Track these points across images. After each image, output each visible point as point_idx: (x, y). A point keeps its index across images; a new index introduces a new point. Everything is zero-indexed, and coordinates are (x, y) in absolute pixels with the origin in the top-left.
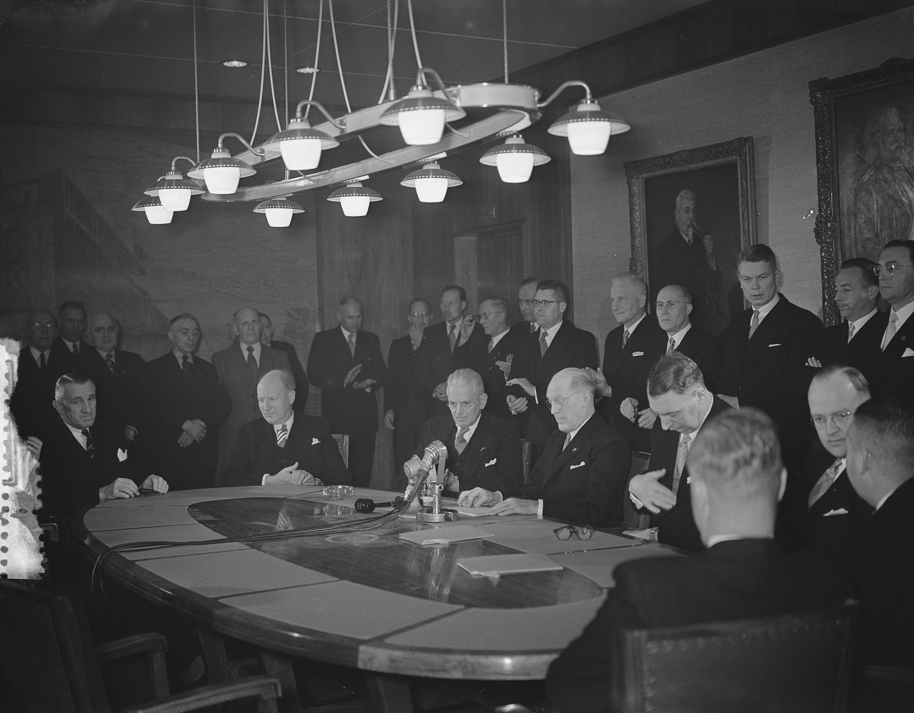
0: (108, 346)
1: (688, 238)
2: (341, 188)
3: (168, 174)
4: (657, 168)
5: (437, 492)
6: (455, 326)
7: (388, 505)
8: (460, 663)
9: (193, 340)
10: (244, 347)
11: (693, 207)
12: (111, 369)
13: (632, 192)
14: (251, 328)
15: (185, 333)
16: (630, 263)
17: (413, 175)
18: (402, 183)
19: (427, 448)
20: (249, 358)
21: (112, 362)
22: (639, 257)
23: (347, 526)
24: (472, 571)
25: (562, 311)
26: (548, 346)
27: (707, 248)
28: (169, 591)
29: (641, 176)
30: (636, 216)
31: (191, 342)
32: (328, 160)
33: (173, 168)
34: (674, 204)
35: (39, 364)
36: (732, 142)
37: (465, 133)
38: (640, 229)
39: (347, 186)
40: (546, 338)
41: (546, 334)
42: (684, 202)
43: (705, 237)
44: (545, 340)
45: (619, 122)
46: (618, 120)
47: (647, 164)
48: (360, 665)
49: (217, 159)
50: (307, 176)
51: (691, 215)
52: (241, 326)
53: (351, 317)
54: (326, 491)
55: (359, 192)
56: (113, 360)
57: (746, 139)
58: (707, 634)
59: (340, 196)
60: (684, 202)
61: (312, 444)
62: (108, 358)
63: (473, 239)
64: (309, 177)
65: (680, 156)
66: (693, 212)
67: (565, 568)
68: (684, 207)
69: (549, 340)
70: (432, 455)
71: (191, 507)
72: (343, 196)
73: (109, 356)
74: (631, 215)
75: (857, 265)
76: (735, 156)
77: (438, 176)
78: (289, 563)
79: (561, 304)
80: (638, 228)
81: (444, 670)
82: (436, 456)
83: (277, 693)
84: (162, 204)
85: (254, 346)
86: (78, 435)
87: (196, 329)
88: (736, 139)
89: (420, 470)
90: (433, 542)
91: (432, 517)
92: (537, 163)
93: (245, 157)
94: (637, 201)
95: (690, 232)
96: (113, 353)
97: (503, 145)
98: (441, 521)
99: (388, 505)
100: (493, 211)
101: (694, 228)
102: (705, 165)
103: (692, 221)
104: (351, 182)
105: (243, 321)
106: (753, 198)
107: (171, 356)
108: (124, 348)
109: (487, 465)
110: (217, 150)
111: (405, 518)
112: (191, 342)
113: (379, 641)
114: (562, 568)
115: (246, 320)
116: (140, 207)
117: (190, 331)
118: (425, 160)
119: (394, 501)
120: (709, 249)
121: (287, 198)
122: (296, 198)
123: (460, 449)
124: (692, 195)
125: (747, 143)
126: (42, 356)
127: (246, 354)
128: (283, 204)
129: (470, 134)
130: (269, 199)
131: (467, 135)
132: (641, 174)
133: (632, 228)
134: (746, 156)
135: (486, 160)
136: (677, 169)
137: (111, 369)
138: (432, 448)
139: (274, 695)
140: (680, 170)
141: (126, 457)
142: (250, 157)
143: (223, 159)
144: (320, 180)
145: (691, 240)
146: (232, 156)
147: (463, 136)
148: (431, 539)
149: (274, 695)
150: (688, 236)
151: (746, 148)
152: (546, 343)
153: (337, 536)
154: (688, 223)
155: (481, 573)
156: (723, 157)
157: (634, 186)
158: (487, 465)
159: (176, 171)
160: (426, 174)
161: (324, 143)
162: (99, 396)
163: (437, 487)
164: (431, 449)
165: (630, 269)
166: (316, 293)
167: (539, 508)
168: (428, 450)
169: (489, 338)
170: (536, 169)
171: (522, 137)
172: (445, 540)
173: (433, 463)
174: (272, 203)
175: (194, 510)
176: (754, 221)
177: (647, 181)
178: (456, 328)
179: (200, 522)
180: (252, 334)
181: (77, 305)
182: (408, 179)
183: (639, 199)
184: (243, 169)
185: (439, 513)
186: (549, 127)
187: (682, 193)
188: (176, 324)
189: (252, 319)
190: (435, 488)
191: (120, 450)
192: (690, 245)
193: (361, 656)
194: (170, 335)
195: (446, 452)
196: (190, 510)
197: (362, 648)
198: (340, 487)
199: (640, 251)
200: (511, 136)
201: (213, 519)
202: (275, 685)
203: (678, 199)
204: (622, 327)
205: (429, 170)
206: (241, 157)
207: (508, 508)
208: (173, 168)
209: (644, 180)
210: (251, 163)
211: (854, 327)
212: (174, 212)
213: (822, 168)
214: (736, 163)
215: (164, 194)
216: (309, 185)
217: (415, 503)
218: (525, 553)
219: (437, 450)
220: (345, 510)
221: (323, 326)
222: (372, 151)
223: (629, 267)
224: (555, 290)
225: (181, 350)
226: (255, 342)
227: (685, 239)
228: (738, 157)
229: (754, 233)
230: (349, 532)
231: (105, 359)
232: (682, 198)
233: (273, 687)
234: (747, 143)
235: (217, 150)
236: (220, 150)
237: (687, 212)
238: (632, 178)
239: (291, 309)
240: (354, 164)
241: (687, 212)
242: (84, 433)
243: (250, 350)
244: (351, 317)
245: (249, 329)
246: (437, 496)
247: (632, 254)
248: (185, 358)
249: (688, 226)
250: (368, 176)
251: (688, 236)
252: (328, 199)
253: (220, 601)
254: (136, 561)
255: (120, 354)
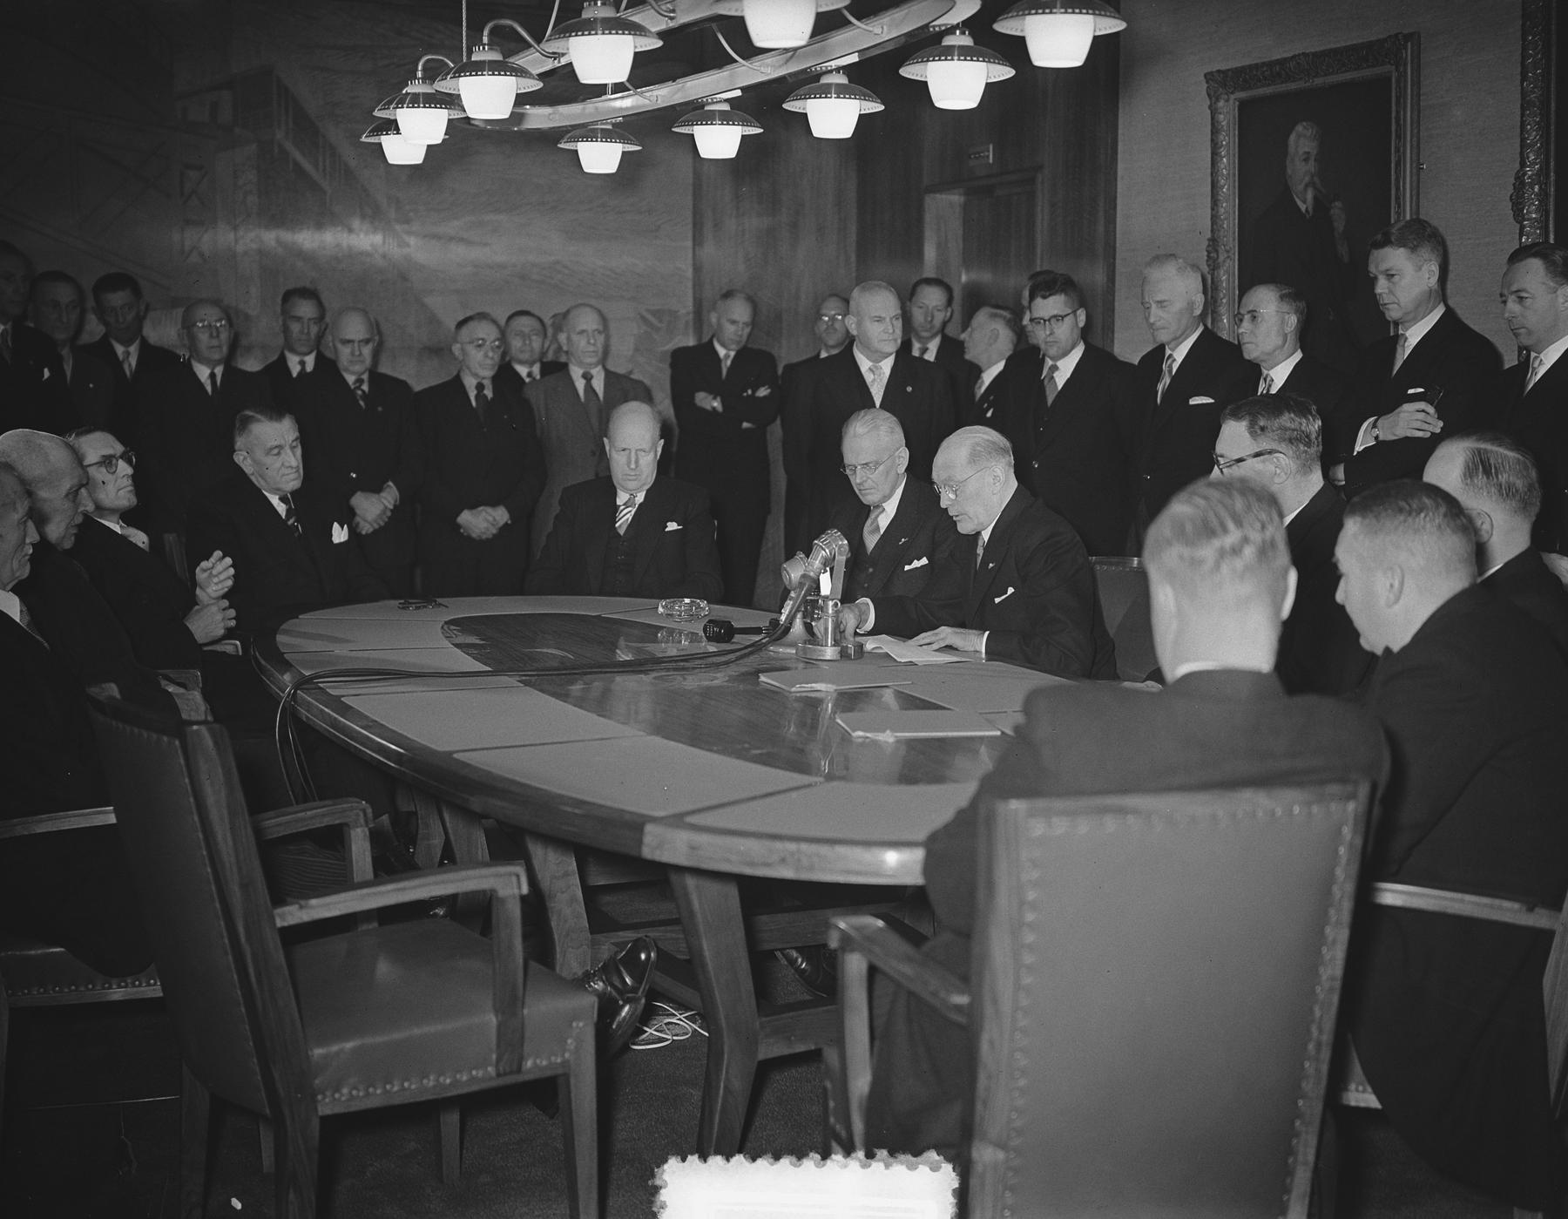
0: (358, 368)
1: (1305, 206)
2: (697, 111)
3: (411, 83)
4: (1259, 84)
5: (830, 611)
6: (927, 349)
7: (757, 631)
8: (792, 854)
9: (492, 358)
10: (576, 372)
11: (1315, 152)
12: (362, 403)
13: (1216, 124)
14: (592, 341)
15: (480, 346)
16: (1209, 246)
17: (802, 93)
18: (784, 106)
19: (816, 542)
20: (586, 391)
21: (363, 391)
22: (1224, 237)
23: (682, 661)
24: (854, 731)
25: (1081, 324)
26: (1060, 388)
27: (1336, 224)
28: (393, 744)
29: (1232, 97)
30: (1222, 166)
31: (489, 362)
32: (646, 70)
33: (419, 74)
34: (1286, 146)
35: (209, 389)
36: (1385, 40)
37: (873, 26)
38: (1228, 189)
39: (706, 108)
40: (1055, 375)
41: (1054, 368)
42: (1302, 142)
43: (1333, 205)
44: (1053, 377)
45: (1105, 16)
46: (1103, 13)
47: (1243, 75)
48: (647, 853)
49: (480, 61)
50: (639, 90)
51: (1311, 166)
52: (575, 338)
53: (734, 322)
54: (663, 607)
55: (726, 118)
56: (365, 387)
57: (1408, 37)
58: (1122, 811)
59: (578, 141)
60: (1302, 142)
61: (667, 530)
62: (358, 385)
63: (957, 198)
64: (643, 92)
65: (1298, 63)
66: (1315, 160)
67: (1003, 733)
68: (1301, 152)
69: (1061, 378)
70: (823, 552)
71: (446, 623)
72: (582, 141)
73: (360, 381)
74: (1214, 164)
75: (1535, 255)
76: (1389, 66)
77: (842, 96)
78: (576, 709)
79: (1079, 312)
80: (1223, 187)
81: (768, 865)
82: (831, 554)
83: (519, 887)
84: (402, 131)
85: (594, 372)
86: (275, 500)
87: (498, 339)
88: (1390, 36)
89: (804, 576)
90: (811, 688)
91: (820, 651)
92: (995, 77)
93: (526, 60)
94: (1225, 140)
95: (1310, 195)
96: (365, 377)
97: (938, 46)
98: (835, 658)
99: (757, 631)
100: (989, 151)
101: (1315, 188)
102: (1340, 79)
103: (1312, 176)
104: (710, 100)
105: (578, 330)
106: (1415, 139)
107: (456, 384)
108: (385, 369)
109: (907, 568)
110: (481, 48)
111: (779, 653)
112: (489, 362)
113: (677, 821)
114: (999, 733)
115: (584, 327)
116: (373, 135)
117: (488, 343)
118: (821, 68)
119: (768, 625)
120: (1339, 225)
121: (614, 125)
122: (625, 128)
123: (871, 541)
124: (1314, 133)
125: (1409, 44)
126: (212, 376)
127: (580, 385)
128: (608, 136)
129: (882, 28)
130: (583, 126)
131: (878, 31)
132: (1232, 93)
133: (1214, 185)
134: (1405, 65)
135: (910, 72)
136: (1293, 86)
137: (362, 403)
138: (826, 540)
139: (516, 891)
140: (1299, 86)
141: (346, 538)
142: (534, 61)
143: (490, 62)
144: (659, 98)
145: (1310, 209)
146: (504, 58)
147: (871, 31)
148: (807, 683)
149: (516, 891)
150: (1305, 203)
151: (1406, 53)
152: (1056, 384)
153: (663, 674)
154: (1307, 179)
155: (868, 735)
156: (1368, 67)
157: (1221, 113)
158: (907, 568)
159: (424, 79)
160: (824, 92)
161: (636, 40)
162: (307, 441)
163: (831, 603)
164: (822, 542)
165: (1208, 256)
166: (690, 284)
167: (979, 642)
168: (818, 545)
169: (976, 371)
170: (990, 88)
171: (969, 34)
172: (829, 686)
173: (825, 565)
174: (588, 132)
175: (452, 627)
176: (1415, 178)
177: (1243, 106)
178: (928, 351)
179: (457, 645)
180: (594, 352)
181: (310, 294)
182: (793, 100)
183: (1228, 135)
184: (521, 80)
185: (831, 646)
186: (994, 21)
187: (1299, 128)
188: (465, 331)
189: (595, 327)
190: (827, 605)
191: (336, 525)
192: (1307, 216)
193: (647, 839)
194: (456, 348)
195: (847, 548)
196: (445, 627)
197: (649, 828)
198: (687, 600)
199: (1225, 226)
200: (951, 30)
201: (478, 642)
202: (518, 876)
203: (1292, 137)
204: (1160, 349)
205: (829, 85)
206: (521, 60)
207: (937, 638)
208: (419, 74)
209: (1237, 103)
210: (535, 72)
211: (1541, 360)
212: (428, 146)
213: (1529, 89)
214: (1390, 79)
215: (405, 116)
216: (644, 106)
217: (798, 626)
218: (944, 708)
219: (833, 545)
220: (693, 637)
221: (700, 338)
222: (733, 50)
223: (1206, 253)
224: (1066, 294)
225: (475, 375)
226: (596, 365)
227: (1301, 207)
228: (1394, 67)
229: (1414, 198)
230: (684, 669)
231: (352, 387)
232: (1299, 136)
233: (514, 879)
234: (1409, 44)
235: (481, 48)
236: (486, 47)
237: (1306, 160)
238: (1218, 100)
239: (648, 310)
240: (711, 72)
241: (1306, 160)
242: (283, 499)
243: (587, 377)
244: (734, 322)
245: (589, 343)
246: (830, 620)
247: (1212, 231)
248: (480, 387)
249: (1307, 186)
250: (739, 91)
251: (1305, 203)
252: (673, 129)
253: (455, 756)
254: (343, 696)
255: (375, 377)
